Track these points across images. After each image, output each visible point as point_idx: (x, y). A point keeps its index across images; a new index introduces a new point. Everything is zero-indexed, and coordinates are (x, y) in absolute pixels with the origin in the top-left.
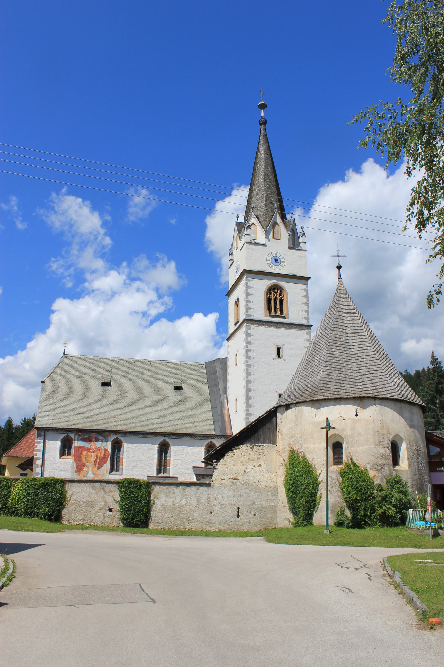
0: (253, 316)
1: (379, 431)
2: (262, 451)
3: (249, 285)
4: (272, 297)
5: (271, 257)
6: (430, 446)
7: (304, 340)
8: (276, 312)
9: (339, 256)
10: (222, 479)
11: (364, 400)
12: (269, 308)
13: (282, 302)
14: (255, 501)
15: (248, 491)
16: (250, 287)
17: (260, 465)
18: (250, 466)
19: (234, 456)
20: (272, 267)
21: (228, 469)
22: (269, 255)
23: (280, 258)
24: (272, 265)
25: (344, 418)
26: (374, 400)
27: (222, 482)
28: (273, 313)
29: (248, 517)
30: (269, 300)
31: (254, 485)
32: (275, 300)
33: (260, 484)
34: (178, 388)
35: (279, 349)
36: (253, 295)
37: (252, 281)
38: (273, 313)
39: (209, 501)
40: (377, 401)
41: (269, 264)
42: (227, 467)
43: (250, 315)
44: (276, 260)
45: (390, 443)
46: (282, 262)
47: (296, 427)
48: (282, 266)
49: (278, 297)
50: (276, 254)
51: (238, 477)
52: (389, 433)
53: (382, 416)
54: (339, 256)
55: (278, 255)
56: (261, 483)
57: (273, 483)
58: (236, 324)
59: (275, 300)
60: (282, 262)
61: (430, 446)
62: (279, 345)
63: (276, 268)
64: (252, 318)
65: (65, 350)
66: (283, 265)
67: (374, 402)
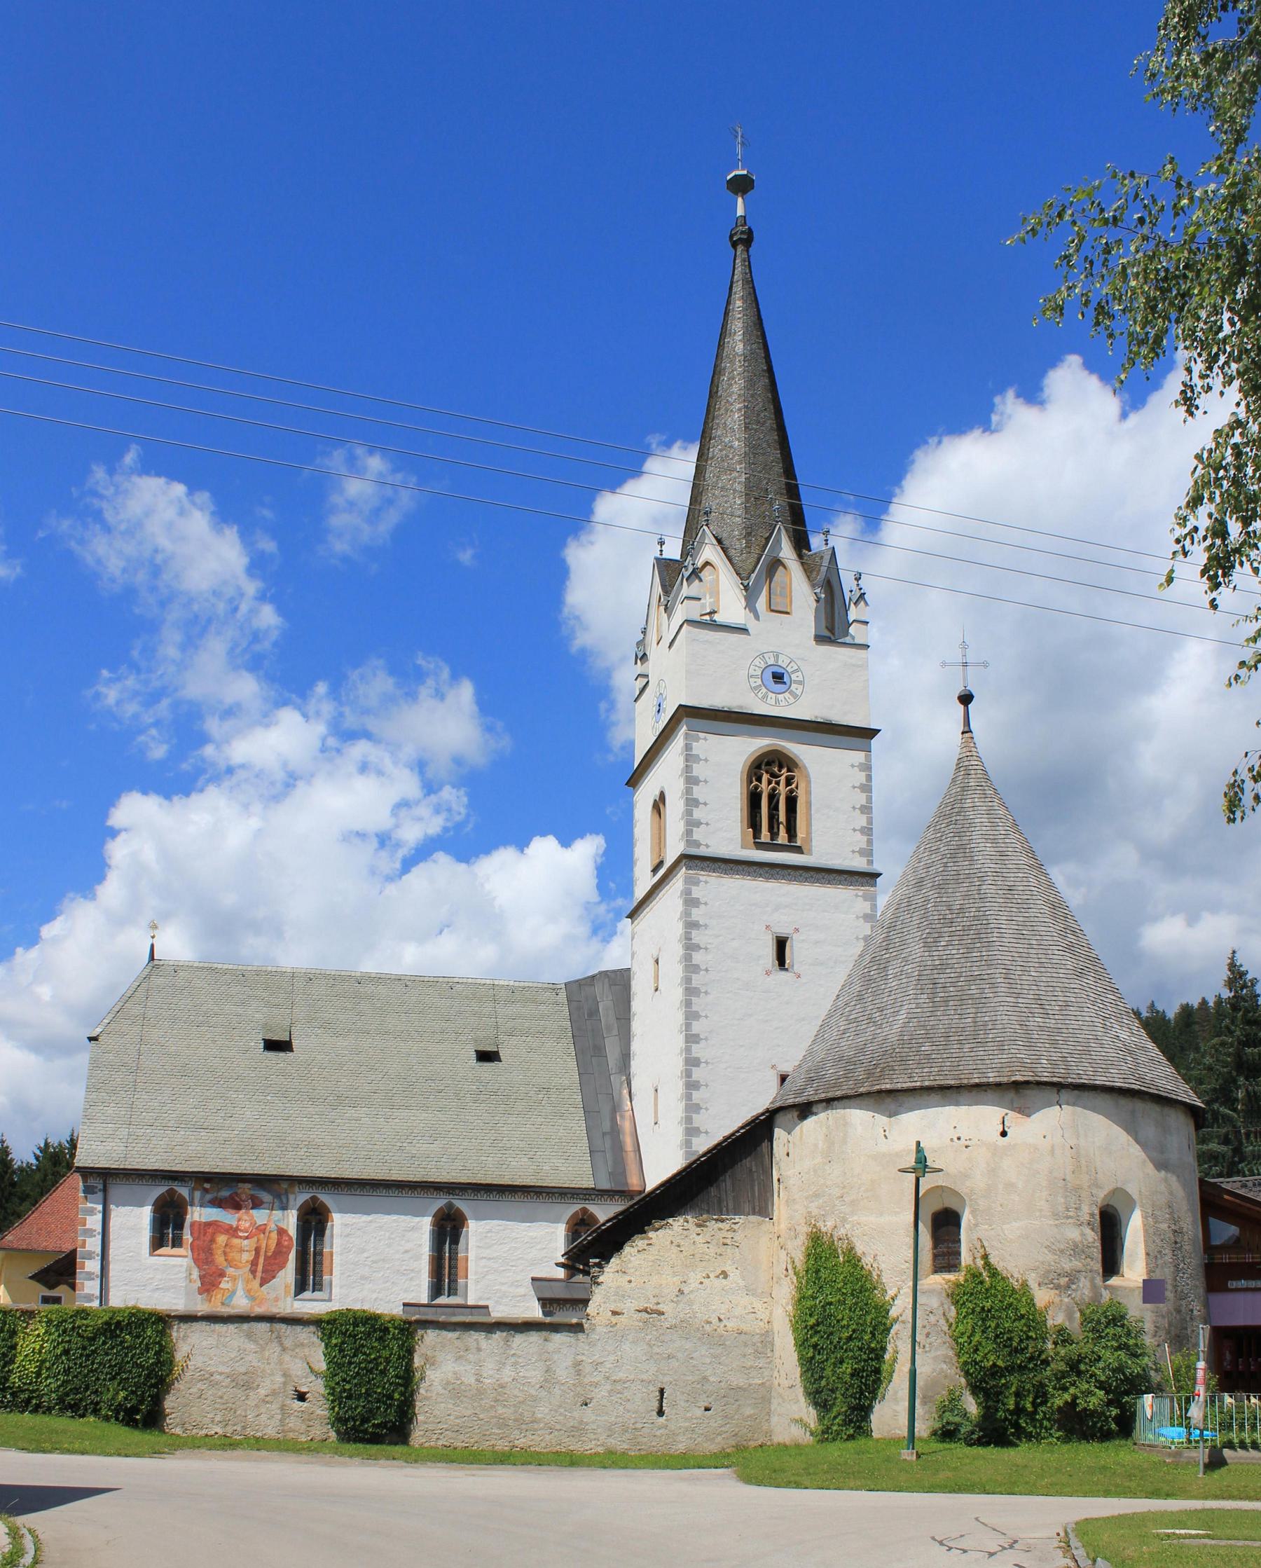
0: (707, 846)
2: (730, 1235)
4: (764, 787)
8: (774, 833)
10: (615, 1313)
11: (1028, 1092)
12: (754, 824)
13: (792, 802)
14: (708, 1373)
15: (688, 1345)
16: (697, 759)
17: (725, 1275)
18: (694, 1277)
19: (651, 1248)
21: (633, 1284)
23: (789, 669)
24: (764, 690)
25: (968, 1143)
26: (1055, 1090)
27: (614, 1319)
28: (765, 836)
29: (689, 1415)
30: (754, 800)
31: (707, 1327)
32: (773, 797)
33: (722, 1325)
37: (705, 739)
38: (765, 836)
39: (579, 1373)
40: (1065, 1095)
41: (755, 688)
42: (628, 1278)
43: (697, 844)
44: (778, 677)
45: (1097, 1212)
46: (796, 682)
48: (795, 696)
49: (782, 790)
50: (777, 657)
51: (660, 1307)
54: (965, 665)
55: (783, 661)
56: (725, 1322)
57: (761, 1324)
58: (655, 870)
59: (773, 797)
61: (1212, 1220)
62: (783, 931)
63: (777, 701)
64: (702, 851)
65: (152, 946)
66: (798, 692)
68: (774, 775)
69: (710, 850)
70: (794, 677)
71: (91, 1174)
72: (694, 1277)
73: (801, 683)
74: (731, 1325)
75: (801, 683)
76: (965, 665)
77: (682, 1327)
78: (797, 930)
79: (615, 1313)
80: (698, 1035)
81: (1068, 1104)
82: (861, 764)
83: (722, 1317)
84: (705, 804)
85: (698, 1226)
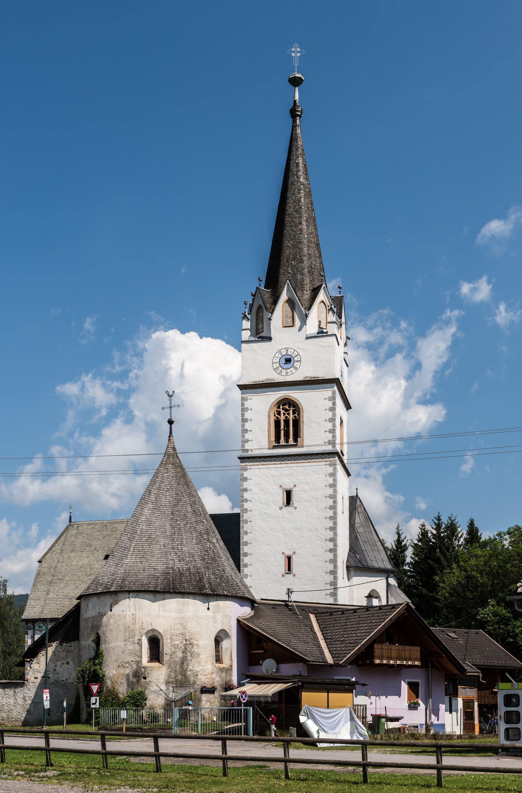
2: (70, 648)
3: (245, 406)
4: (282, 418)
5: (280, 356)
7: (326, 475)
8: (287, 439)
9: (171, 407)
11: (119, 594)
15: (57, 689)
16: (247, 409)
17: (68, 663)
18: (59, 664)
20: (281, 372)
22: (277, 355)
23: (293, 355)
24: (280, 369)
26: (128, 593)
30: (277, 423)
31: (63, 682)
32: (287, 422)
35: (289, 494)
37: (251, 399)
38: (282, 442)
40: (131, 595)
41: (276, 369)
43: (247, 451)
48: (296, 368)
49: (291, 417)
59: (287, 422)
62: (288, 487)
63: (287, 373)
64: (250, 454)
65: (70, 516)
66: (298, 366)
67: (128, 596)
68: (286, 410)
69: (253, 453)
71: (29, 621)
73: (299, 361)
74: (70, 681)
75: (299, 361)
78: (295, 486)
81: (132, 597)
82: (330, 397)
84: (251, 431)
85: (60, 645)
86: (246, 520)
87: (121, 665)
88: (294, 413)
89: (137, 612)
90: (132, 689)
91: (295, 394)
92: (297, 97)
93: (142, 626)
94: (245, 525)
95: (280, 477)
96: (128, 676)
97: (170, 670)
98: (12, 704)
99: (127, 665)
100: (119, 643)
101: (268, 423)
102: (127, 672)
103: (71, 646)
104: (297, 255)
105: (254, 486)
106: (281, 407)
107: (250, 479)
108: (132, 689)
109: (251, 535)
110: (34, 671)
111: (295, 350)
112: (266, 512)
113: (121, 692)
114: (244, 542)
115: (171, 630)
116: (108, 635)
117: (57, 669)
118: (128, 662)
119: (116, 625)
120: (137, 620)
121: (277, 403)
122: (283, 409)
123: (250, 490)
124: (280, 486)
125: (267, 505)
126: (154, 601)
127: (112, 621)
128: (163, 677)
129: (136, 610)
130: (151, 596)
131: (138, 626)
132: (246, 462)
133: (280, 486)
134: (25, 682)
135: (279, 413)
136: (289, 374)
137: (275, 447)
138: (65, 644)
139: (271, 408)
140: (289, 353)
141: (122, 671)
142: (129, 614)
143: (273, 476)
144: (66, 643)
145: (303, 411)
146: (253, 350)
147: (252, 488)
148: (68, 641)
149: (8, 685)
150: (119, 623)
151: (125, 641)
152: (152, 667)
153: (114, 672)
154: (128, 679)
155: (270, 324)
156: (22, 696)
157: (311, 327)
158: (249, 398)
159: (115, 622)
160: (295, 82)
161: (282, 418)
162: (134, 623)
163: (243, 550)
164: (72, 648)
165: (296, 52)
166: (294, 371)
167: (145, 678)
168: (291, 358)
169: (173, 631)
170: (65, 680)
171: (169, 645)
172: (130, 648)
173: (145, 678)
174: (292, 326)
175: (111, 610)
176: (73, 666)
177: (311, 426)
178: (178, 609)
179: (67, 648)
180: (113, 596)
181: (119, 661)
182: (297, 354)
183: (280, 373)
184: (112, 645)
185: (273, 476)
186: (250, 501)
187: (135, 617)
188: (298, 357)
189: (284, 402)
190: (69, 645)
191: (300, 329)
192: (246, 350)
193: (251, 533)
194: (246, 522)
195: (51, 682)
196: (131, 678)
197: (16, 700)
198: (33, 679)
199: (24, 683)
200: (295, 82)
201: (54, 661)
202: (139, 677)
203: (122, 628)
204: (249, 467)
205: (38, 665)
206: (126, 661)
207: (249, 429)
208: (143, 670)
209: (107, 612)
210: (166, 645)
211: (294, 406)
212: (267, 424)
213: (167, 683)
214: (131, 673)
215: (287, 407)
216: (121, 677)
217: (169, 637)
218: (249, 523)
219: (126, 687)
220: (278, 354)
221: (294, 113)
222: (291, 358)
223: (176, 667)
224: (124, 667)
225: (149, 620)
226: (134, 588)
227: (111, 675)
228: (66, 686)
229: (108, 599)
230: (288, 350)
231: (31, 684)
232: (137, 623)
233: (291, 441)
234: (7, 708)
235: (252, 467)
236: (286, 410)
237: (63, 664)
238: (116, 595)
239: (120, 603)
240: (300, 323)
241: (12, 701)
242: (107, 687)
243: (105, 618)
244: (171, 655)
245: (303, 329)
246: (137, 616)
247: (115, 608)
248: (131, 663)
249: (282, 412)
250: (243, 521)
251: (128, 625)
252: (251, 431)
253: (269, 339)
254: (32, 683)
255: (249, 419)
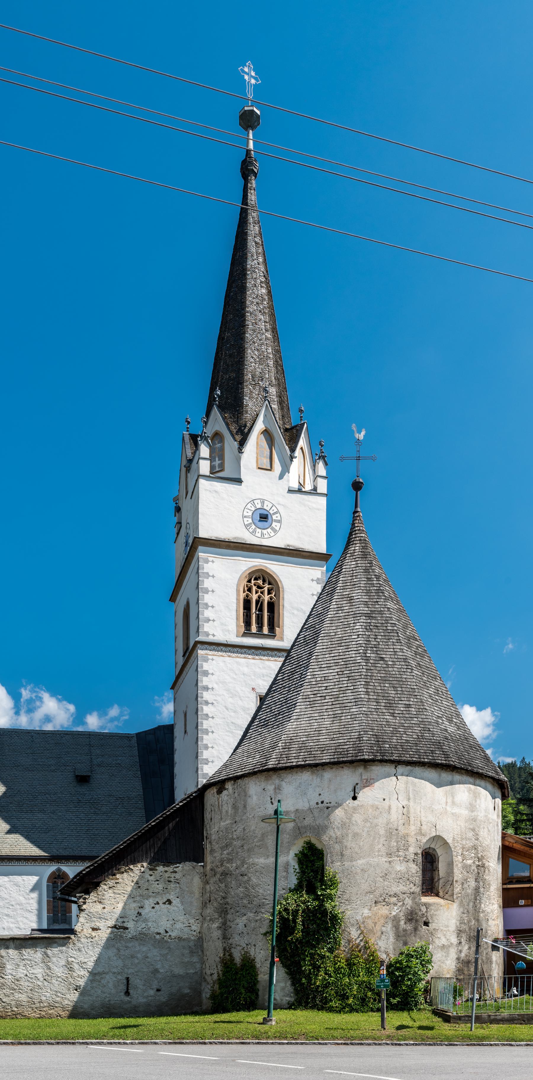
0: (214, 635)
1: (399, 828)
2: (173, 875)
4: (254, 597)
5: (253, 509)
6: (511, 861)
8: (260, 627)
10: (94, 929)
11: (374, 768)
12: (248, 624)
13: (271, 606)
14: (159, 966)
17: (169, 902)
18: (148, 903)
19: (118, 885)
21: (105, 910)
24: (253, 527)
25: (329, 805)
27: (94, 934)
28: (254, 629)
29: (145, 994)
30: (247, 603)
31: (158, 937)
33: (168, 934)
34: (83, 780)
36: (213, 591)
37: (213, 562)
38: (254, 629)
39: (71, 969)
40: (401, 769)
42: (103, 906)
44: (264, 517)
45: (420, 852)
46: (276, 521)
47: (235, 825)
48: (275, 531)
49: (266, 598)
50: (263, 502)
51: (125, 925)
52: (420, 833)
53: (409, 799)
54: (358, 458)
55: (267, 506)
56: (170, 933)
57: (195, 933)
58: (184, 656)
60: (276, 521)
61: (511, 861)
63: (262, 534)
66: (277, 528)
69: (215, 638)
70: (274, 517)
72: (148, 903)
74: (173, 934)
75: (279, 521)
76: (358, 458)
77: (142, 937)
79: (94, 929)
80: (207, 760)
81: (402, 775)
83: (168, 930)
84: (213, 607)
85: (151, 869)
86: (207, 729)
87: (380, 899)
88: (269, 593)
89: (411, 804)
90: (405, 944)
91: (275, 567)
92: (251, 146)
93: (420, 829)
94: (205, 737)
95: (253, 677)
96: (396, 920)
97: (462, 910)
98: (40, 976)
99: (394, 900)
100: (376, 860)
101: (237, 599)
102: (394, 913)
103: (175, 872)
104: (265, 374)
105: (217, 683)
106: (253, 582)
107: (212, 674)
108: (405, 944)
109: (213, 751)
110: (90, 917)
111: (273, 505)
112: (233, 721)
113: (382, 949)
114: (203, 759)
115: (462, 839)
116: (349, 843)
117: (143, 912)
118: (395, 895)
119: (368, 824)
120: (412, 819)
121: (249, 574)
122: (255, 585)
123: (213, 689)
124: (253, 689)
125: (235, 712)
126: (439, 785)
127: (358, 818)
128: (454, 921)
129: (409, 799)
130: (432, 773)
131: (413, 829)
132: (206, 649)
133: (253, 689)
134: (72, 936)
135: (250, 590)
136: (266, 536)
137: (244, 635)
138: (161, 868)
139: (240, 580)
140: (265, 507)
141: (383, 910)
142: (396, 806)
143: (244, 674)
144: (164, 866)
145: (283, 591)
146: (216, 492)
147: (215, 686)
148: (167, 863)
149: (30, 942)
150: (375, 821)
151: (389, 855)
152: (438, 904)
153: (366, 912)
154: (396, 927)
155: (240, 458)
156: (63, 963)
157: (293, 480)
158: (210, 559)
159: (366, 821)
160: (248, 120)
161: (254, 597)
162: (407, 822)
163: (202, 769)
164: (178, 876)
165: (250, 77)
166: (272, 534)
167: (426, 924)
168: (267, 515)
169: (464, 842)
170: (162, 931)
171: (460, 865)
172: (398, 868)
173: (426, 924)
174: (270, 470)
175: (355, 798)
176: (182, 908)
177: (293, 613)
178: (470, 804)
179: (167, 875)
180: (361, 770)
181: (377, 893)
182: (276, 510)
183: (253, 533)
184: (360, 862)
185: (244, 674)
186: (212, 704)
187: (408, 812)
188: (278, 515)
189: (257, 575)
190: (170, 869)
191: (281, 477)
192: (206, 490)
193: (212, 747)
194: (206, 732)
195: (130, 936)
196: (402, 923)
197: (50, 969)
198: (87, 931)
199: (69, 938)
200: (248, 120)
201: (138, 898)
202: (417, 921)
203: (382, 832)
204: (210, 657)
205: (100, 907)
206: (392, 893)
207: (210, 604)
208: (424, 909)
209: (344, 800)
210: (457, 865)
211: (269, 584)
212: (235, 601)
213: (459, 932)
214: (402, 914)
215: (260, 582)
216: (382, 921)
217: (460, 852)
218: (210, 734)
219: (392, 939)
220: (250, 504)
221: (246, 170)
222: (267, 515)
223: (468, 905)
224: (388, 904)
225: (432, 818)
226: (407, 758)
227: (359, 918)
228: (167, 942)
229: (348, 777)
230: (263, 503)
231: (82, 940)
232: (412, 822)
233: (266, 630)
234: (27, 984)
235: (214, 657)
236: (259, 587)
237: (158, 903)
238: (365, 767)
239: (377, 784)
240: (280, 469)
241: (39, 971)
242: (349, 941)
243: (339, 813)
244: (463, 884)
245: (285, 477)
246: (412, 810)
247: (365, 795)
248: (402, 896)
249: (254, 588)
250: (202, 730)
251: (395, 827)
252: (213, 607)
253: (238, 481)
254: (87, 938)
255: (210, 589)
